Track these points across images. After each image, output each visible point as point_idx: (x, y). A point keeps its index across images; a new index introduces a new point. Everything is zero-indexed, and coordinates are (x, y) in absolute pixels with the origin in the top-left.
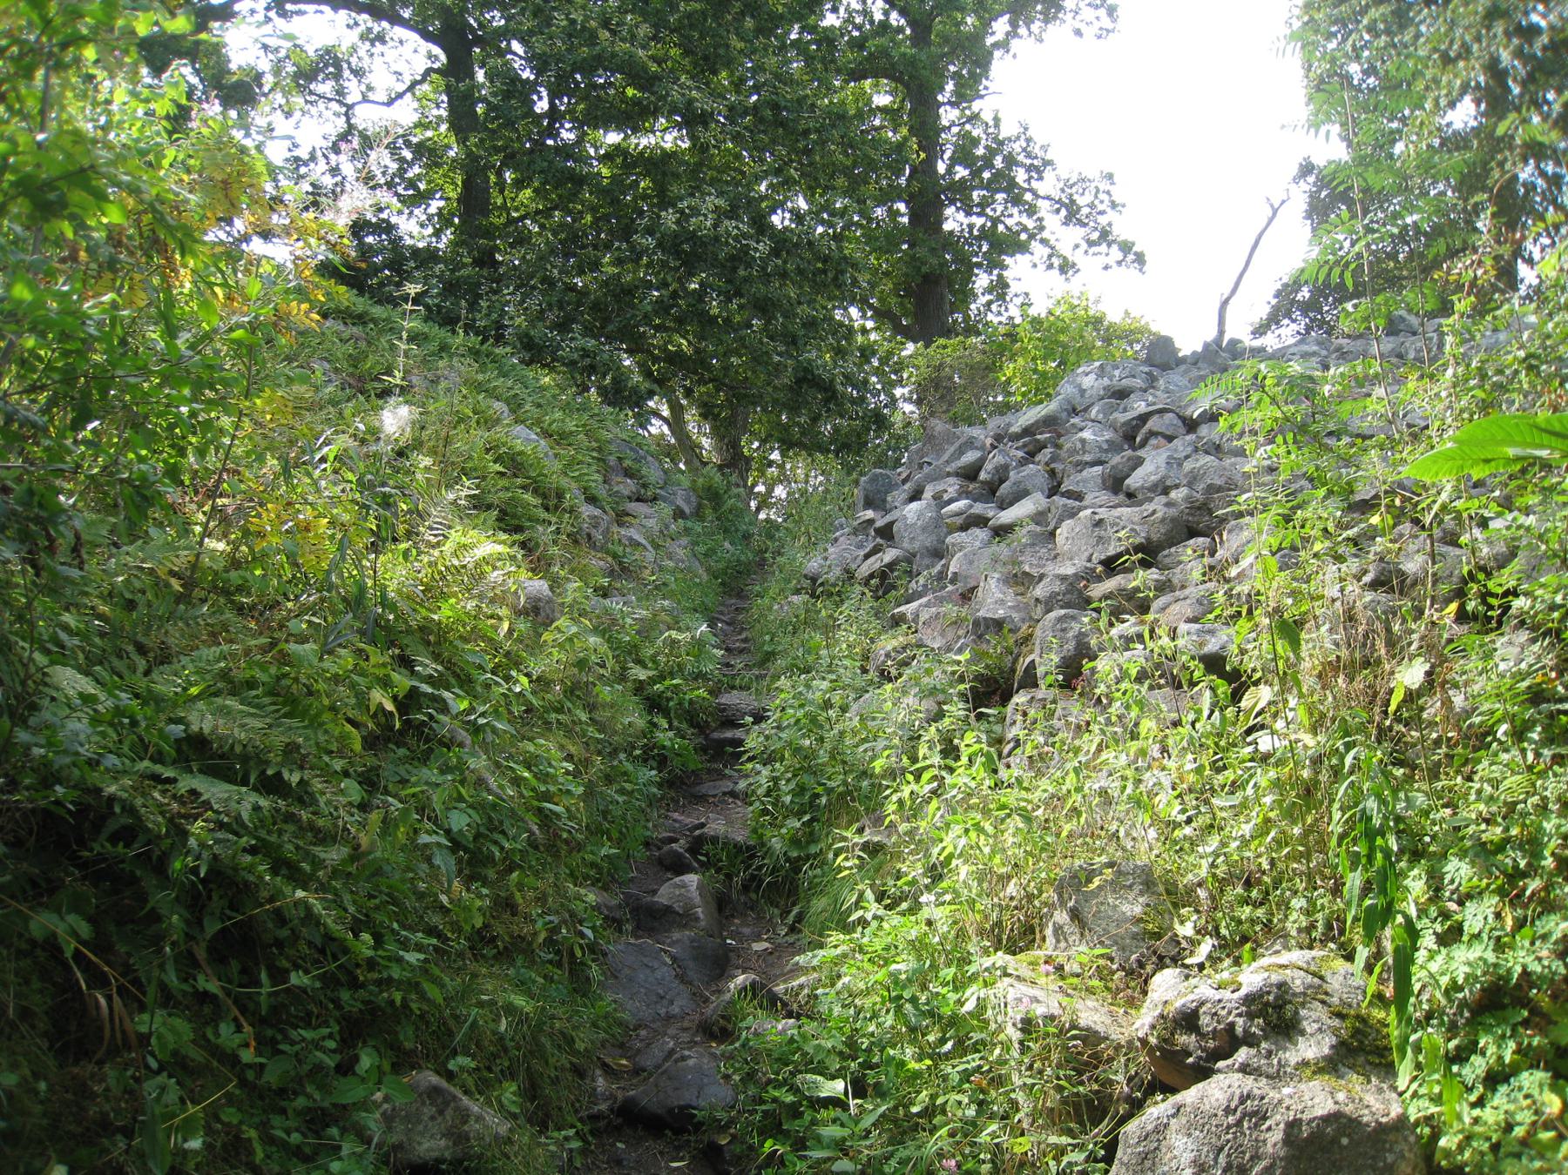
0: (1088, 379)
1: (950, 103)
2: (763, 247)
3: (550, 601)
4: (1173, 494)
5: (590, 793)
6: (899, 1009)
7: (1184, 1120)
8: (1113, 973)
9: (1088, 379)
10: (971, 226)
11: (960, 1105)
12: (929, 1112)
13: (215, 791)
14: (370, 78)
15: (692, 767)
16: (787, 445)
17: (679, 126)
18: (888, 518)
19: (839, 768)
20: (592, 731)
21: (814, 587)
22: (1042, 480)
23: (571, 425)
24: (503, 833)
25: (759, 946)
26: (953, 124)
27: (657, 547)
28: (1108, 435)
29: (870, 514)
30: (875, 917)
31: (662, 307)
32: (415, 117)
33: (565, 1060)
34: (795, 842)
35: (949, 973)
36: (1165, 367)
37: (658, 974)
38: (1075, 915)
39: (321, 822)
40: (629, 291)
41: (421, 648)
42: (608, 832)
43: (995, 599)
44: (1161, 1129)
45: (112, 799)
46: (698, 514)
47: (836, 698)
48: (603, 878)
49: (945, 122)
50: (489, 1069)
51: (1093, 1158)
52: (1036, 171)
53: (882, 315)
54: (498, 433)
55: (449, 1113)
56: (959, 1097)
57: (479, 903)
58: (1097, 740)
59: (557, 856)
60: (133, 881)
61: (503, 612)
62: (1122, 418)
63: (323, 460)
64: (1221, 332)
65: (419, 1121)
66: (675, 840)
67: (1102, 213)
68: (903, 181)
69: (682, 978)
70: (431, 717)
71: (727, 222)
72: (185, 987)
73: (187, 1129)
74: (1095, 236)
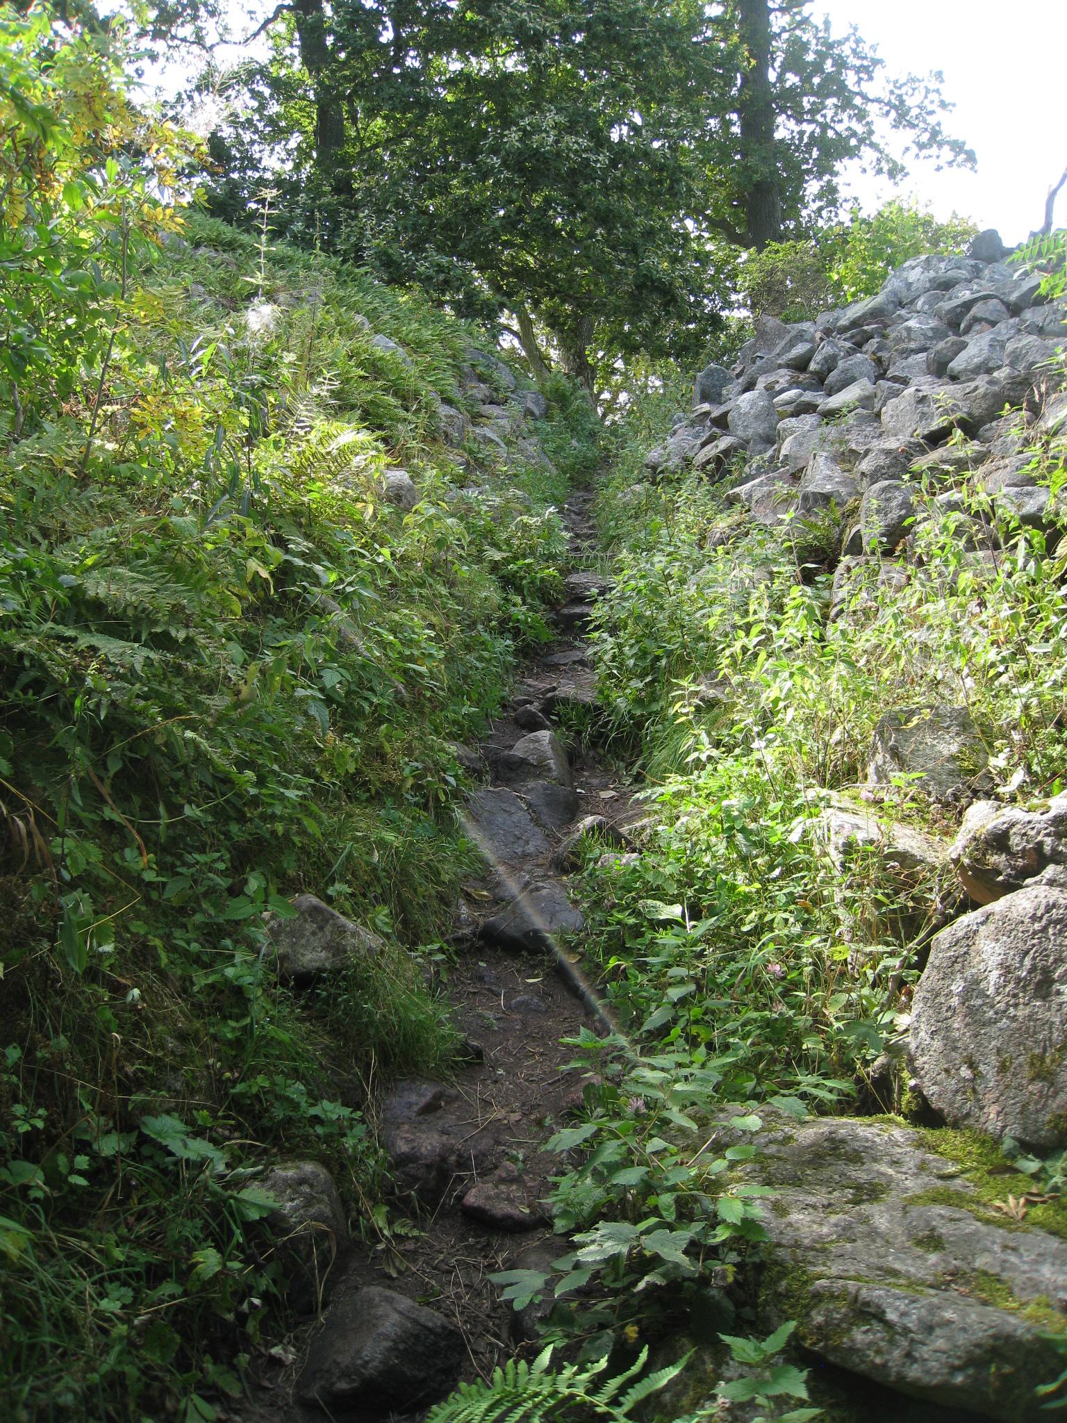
0: (915, 274)
1: (781, 9)
2: (603, 159)
3: (410, 489)
4: (995, 374)
5: (450, 659)
6: (730, 839)
7: (992, 927)
8: (929, 805)
9: (915, 274)
10: (802, 133)
11: (785, 922)
12: (758, 931)
13: (111, 647)
14: (227, 19)
15: (544, 639)
16: (630, 349)
17: (518, 49)
18: (723, 409)
19: (678, 632)
20: (452, 604)
21: (655, 475)
22: (869, 367)
23: (427, 334)
24: (372, 690)
25: (606, 795)
26: (784, 30)
27: (509, 443)
28: (933, 323)
29: (706, 407)
30: (710, 758)
31: (510, 224)
32: (272, 53)
33: (432, 889)
34: (638, 702)
35: (775, 807)
36: (991, 260)
37: (515, 818)
38: (895, 753)
39: (204, 672)
40: (477, 210)
41: (294, 529)
42: (468, 693)
43: (823, 476)
44: (971, 935)
45: (21, 655)
46: (547, 416)
47: (675, 570)
48: (464, 734)
49: (776, 29)
50: (364, 896)
51: (907, 965)
52: (866, 71)
53: (718, 226)
54: (359, 342)
55: (328, 928)
56: (787, 915)
57: (351, 750)
58: (917, 596)
59: (421, 713)
60: (45, 725)
61: (368, 497)
62: (947, 305)
63: (198, 363)
64: (1048, 224)
65: (303, 936)
66: (531, 703)
67: (931, 113)
68: (734, 92)
69: (537, 822)
70: (304, 588)
71: (567, 138)
72: (93, 816)
73: (101, 935)
74: (925, 137)
